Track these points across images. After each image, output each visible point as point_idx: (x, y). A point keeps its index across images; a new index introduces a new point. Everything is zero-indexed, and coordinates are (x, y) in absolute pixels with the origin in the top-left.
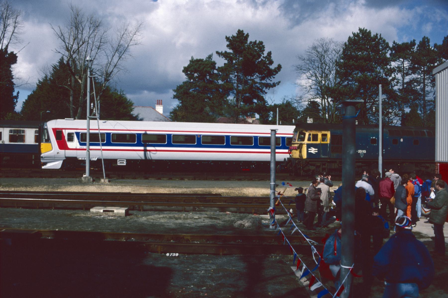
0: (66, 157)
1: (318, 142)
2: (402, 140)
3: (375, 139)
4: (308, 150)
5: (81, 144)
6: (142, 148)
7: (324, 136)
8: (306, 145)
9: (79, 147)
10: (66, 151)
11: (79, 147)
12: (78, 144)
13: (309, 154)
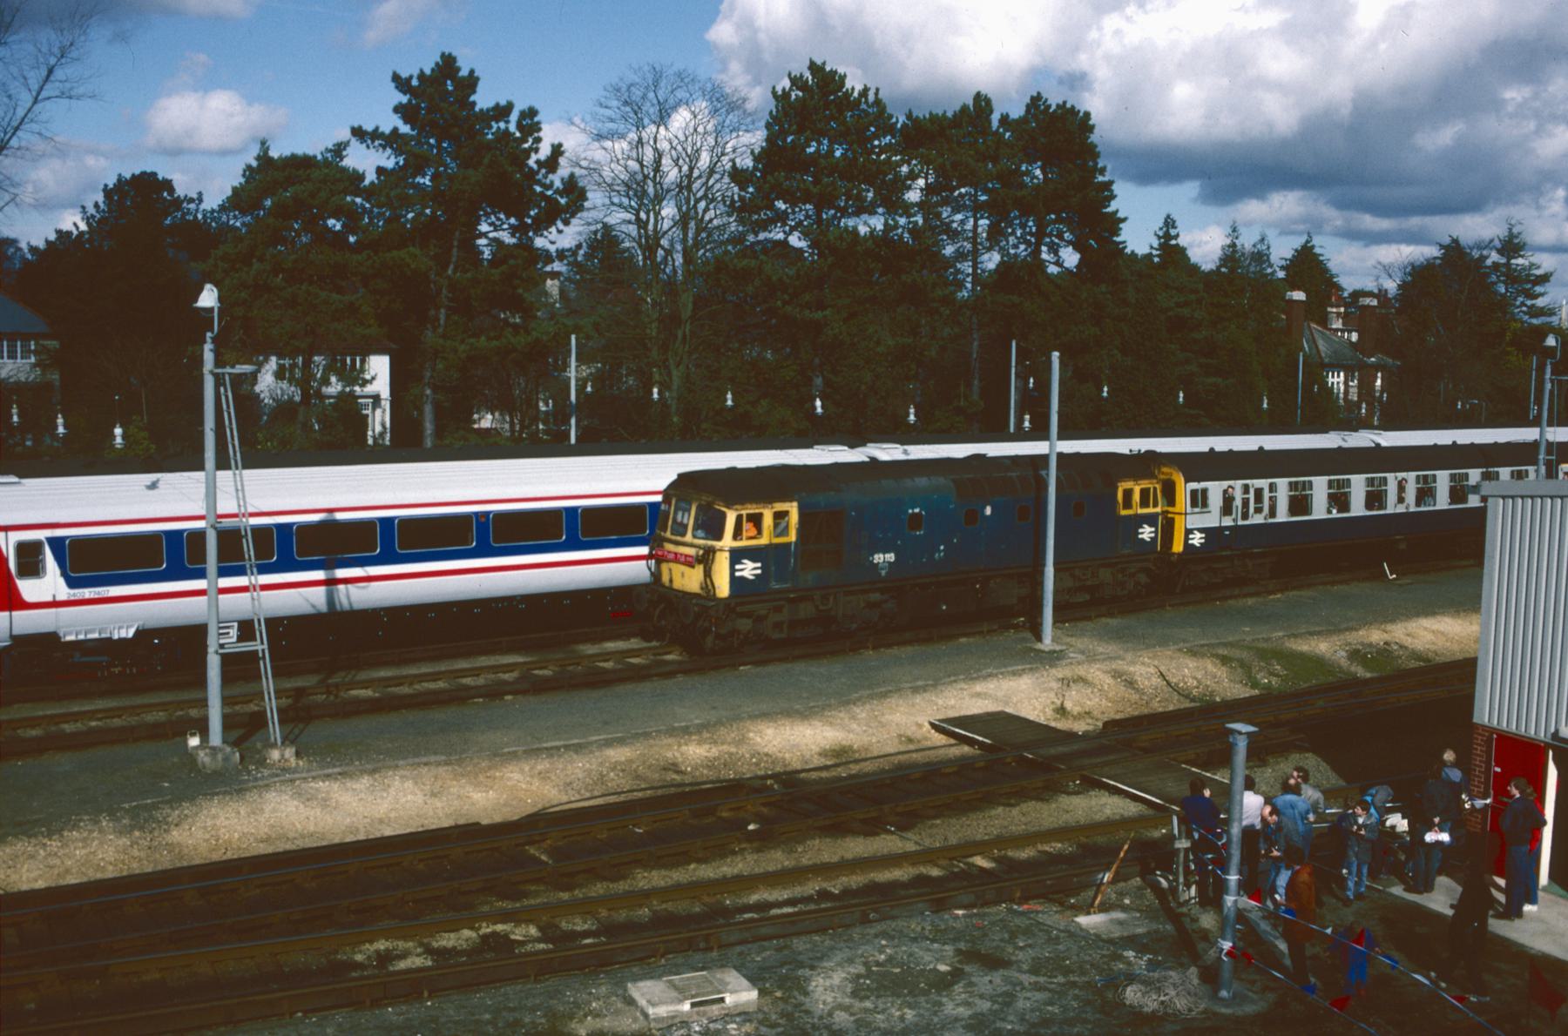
0: (12, 637)
1: (764, 541)
2: (988, 511)
3: (919, 514)
4: (732, 571)
5: (72, 583)
6: (319, 575)
7: (780, 516)
8: (727, 555)
9: (64, 592)
10: (15, 613)
11: (64, 592)
12: (61, 581)
13: (736, 582)
